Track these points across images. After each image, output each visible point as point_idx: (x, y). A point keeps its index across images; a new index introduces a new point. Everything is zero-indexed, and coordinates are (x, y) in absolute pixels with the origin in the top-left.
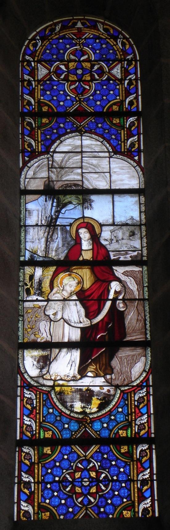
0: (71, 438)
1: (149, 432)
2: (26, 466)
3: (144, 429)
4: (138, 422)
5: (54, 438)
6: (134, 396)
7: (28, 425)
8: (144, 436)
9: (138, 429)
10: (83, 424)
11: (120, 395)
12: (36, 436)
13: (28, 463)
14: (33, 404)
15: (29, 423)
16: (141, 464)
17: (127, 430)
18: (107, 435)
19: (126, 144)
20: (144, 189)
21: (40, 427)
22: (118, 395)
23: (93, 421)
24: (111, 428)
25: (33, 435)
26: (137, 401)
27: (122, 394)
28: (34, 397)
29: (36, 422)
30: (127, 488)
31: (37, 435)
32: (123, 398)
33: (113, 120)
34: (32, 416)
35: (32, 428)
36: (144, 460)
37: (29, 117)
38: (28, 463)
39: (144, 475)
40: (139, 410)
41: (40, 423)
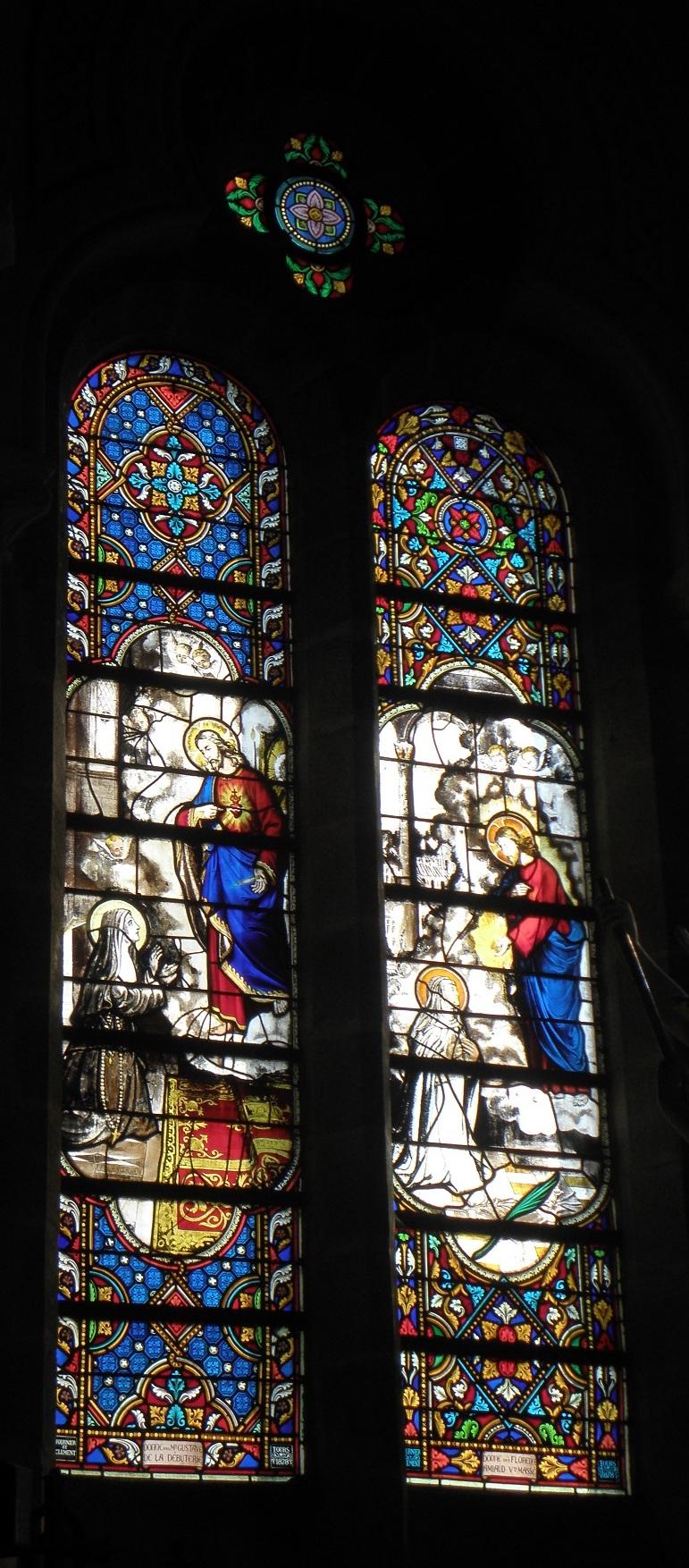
0: (148, 1302)
1: (294, 1302)
2: (64, 1240)
3: (274, 491)
4: (275, 1398)
5: (122, 563)
6: (261, 572)
7: (75, 592)
8: (286, 1309)
9: (276, 1411)
10: (172, 1277)
11: (241, 1219)
12: (81, 1296)
13: (68, 1349)
14: (89, 412)
15: (67, 1269)
16: (280, 1366)
17: (252, 1294)
18: (216, 1303)
19: (266, 1227)
20: (301, 1486)
21: (98, 542)
22: (237, 1220)
23: (191, 1272)
24: (224, 1287)
25: (74, 1294)
26: (266, 580)
27: (244, 1217)
28: (74, 1389)
29: (89, 537)
30: (248, 1395)
31: (84, 1294)
32: (246, 1225)
33: (241, 1332)
34: (81, 524)
35: (71, 1395)
36: (283, 1359)
37: (70, 554)
38: (68, 1349)
39: (270, 521)
40: (268, 549)
41: (97, 536)
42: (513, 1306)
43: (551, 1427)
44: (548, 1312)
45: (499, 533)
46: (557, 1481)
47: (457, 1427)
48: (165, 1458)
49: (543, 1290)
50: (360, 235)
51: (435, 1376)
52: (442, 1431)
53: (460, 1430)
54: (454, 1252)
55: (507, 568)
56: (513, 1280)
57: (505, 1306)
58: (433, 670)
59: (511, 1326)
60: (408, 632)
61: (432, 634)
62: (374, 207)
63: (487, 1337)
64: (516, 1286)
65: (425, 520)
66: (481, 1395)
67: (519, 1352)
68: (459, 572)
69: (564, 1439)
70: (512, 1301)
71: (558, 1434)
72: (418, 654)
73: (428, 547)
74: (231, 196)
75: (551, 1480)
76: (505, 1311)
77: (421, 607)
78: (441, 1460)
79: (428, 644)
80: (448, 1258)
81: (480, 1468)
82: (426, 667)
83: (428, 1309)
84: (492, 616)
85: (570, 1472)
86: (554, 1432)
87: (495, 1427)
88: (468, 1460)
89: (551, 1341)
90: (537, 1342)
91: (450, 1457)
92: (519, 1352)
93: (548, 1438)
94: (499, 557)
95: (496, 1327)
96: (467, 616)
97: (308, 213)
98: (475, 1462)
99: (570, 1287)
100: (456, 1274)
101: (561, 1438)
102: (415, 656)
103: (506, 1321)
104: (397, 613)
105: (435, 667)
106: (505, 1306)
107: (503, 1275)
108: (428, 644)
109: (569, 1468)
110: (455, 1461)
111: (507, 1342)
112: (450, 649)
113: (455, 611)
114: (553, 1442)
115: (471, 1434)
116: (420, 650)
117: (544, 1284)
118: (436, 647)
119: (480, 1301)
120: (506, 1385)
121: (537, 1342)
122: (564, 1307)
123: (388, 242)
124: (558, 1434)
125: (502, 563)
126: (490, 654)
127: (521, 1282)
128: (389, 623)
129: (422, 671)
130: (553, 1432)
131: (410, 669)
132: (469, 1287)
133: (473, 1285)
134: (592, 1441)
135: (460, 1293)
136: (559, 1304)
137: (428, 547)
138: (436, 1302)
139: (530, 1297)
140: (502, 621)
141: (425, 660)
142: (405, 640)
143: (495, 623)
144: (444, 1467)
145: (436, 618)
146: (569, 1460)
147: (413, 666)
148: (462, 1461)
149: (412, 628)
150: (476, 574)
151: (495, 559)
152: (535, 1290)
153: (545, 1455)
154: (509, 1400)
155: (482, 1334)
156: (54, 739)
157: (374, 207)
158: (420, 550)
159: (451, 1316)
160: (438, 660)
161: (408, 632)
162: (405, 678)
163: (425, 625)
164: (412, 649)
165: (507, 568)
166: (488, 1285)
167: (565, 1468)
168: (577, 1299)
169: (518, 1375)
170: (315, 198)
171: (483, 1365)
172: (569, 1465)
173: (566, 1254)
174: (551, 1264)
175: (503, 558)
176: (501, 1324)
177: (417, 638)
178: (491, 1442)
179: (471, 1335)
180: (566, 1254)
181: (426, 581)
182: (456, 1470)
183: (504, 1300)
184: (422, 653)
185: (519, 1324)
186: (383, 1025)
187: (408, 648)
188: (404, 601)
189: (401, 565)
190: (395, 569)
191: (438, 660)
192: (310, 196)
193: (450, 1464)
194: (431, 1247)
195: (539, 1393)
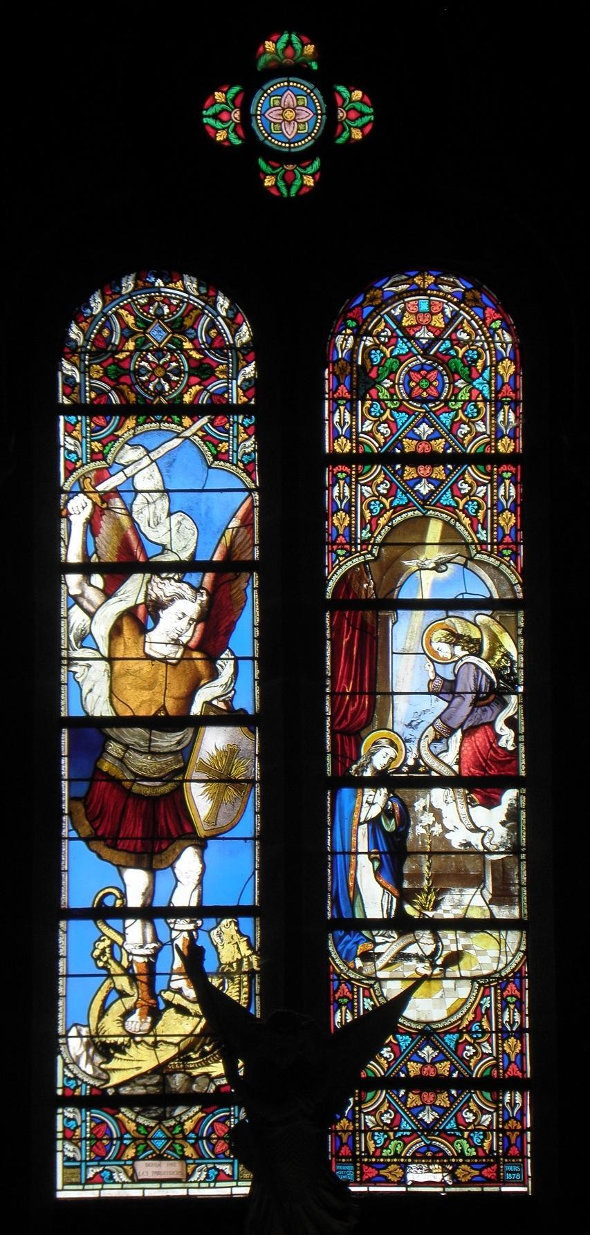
42: (435, 1048)
43: (465, 1142)
44: (465, 1050)
45: (455, 387)
46: (470, 1183)
47: (385, 1147)
50: (332, 125)
51: (365, 1108)
52: (372, 1149)
53: (387, 1148)
54: (467, 530)
55: (461, 419)
56: (434, 1027)
57: (428, 1049)
58: (463, 1017)
59: (433, 1063)
61: (388, 490)
62: (346, 93)
65: (386, 386)
66: (405, 1120)
68: (416, 430)
70: (435, 1044)
71: (471, 1147)
73: (388, 411)
74: (284, 191)
75: (465, 1182)
76: (428, 1052)
77: (380, 467)
78: (371, 1172)
79: (469, 1039)
81: (404, 1177)
82: (470, 1017)
83: (489, 486)
84: (445, 466)
85: (481, 1175)
86: (468, 1146)
87: (417, 1144)
88: (393, 1172)
90: (398, 466)
91: (378, 1170)
93: (462, 1150)
94: (453, 410)
95: (433, 323)
97: (289, 122)
98: (400, 1173)
101: (473, 1149)
103: (424, 328)
104: (358, 475)
105: (461, 1019)
106: (428, 1049)
107: (428, 1023)
108: (469, 1039)
109: (481, 1173)
110: (382, 1172)
111: (428, 1092)
113: (411, 466)
114: (467, 1154)
115: (396, 1151)
116: (476, 1032)
118: (461, 1037)
121: (455, 1075)
123: (356, 127)
125: (456, 416)
128: (350, 486)
129: (378, 525)
130: (466, 1146)
131: (366, 524)
133: (450, 506)
134: (501, 1151)
137: (388, 411)
138: (481, 490)
139: (451, 1039)
140: (454, 469)
143: (448, 472)
144: (373, 1177)
145: (393, 475)
146: (480, 1166)
147: (370, 522)
148: (390, 1172)
151: (449, 412)
152: (453, 1033)
154: (428, 1047)
155: (407, 1073)
156: (128, 582)
157: (346, 93)
158: (382, 415)
159: (470, 481)
162: (361, 533)
164: (484, 1032)
165: (461, 419)
167: (477, 1173)
168: (491, 1036)
170: (289, 98)
171: (407, 1097)
172: (481, 1170)
173: (482, 1002)
174: (468, 1012)
175: (457, 410)
176: (424, 1063)
177: (374, 496)
178: (413, 1157)
179: (398, 1073)
180: (482, 1002)
181: (468, 1101)
182: (383, 1179)
183: (428, 1044)
184: (474, 1030)
185: (440, 1062)
190: (497, 1110)
191: (393, 513)
192: (295, 130)
193: (378, 1175)
195: (455, 1115)
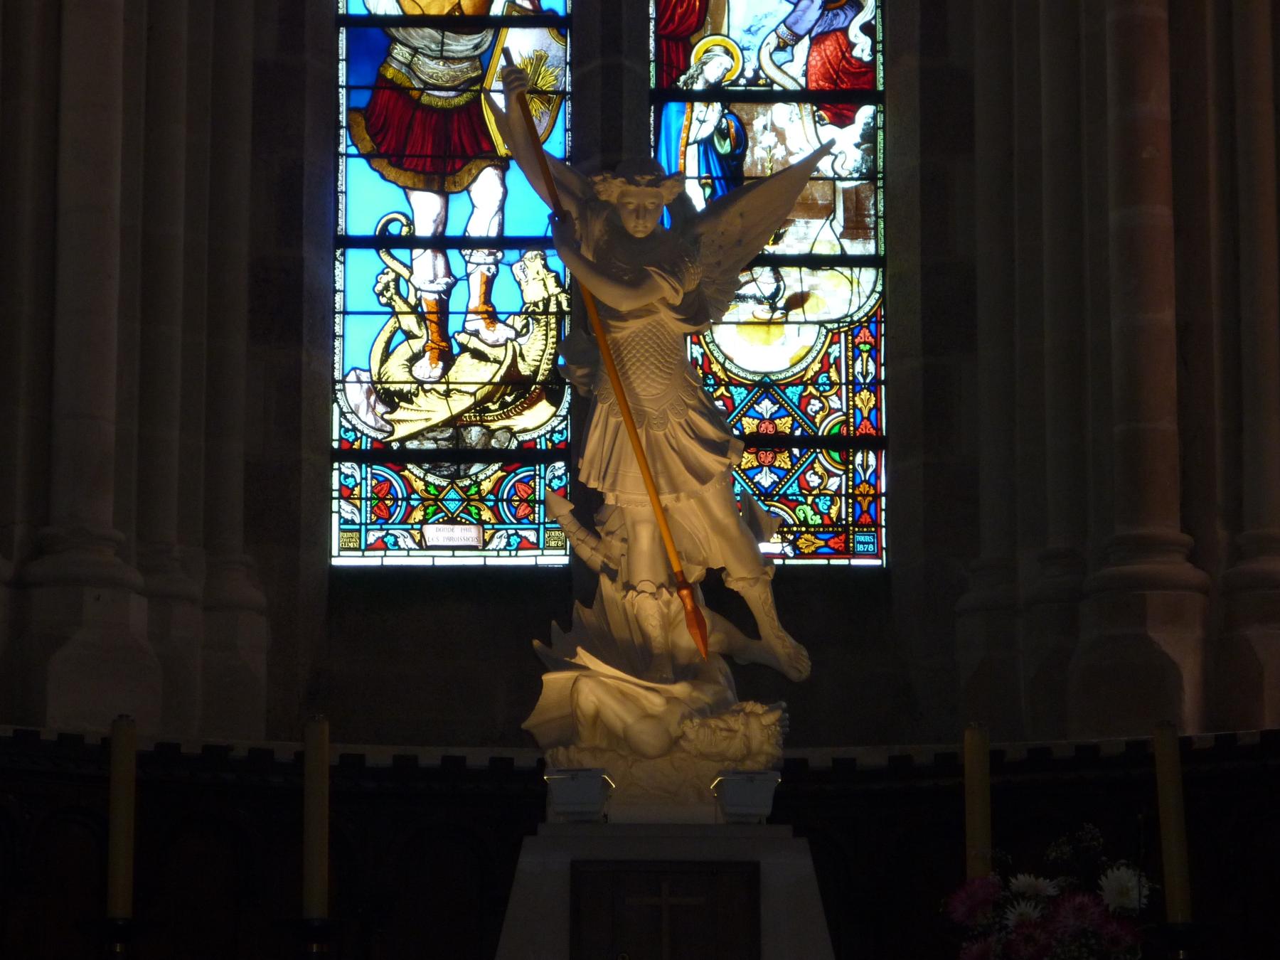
48: (435, 539)
49: (806, 385)
56: (774, 378)
59: (772, 419)
60: (835, 403)
63: (747, 431)
64: (774, 383)
67: (778, 442)
69: (822, 518)
71: (815, 514)
72: (825, 379)
75: (809, 554)
77: (820, 434)
80: (710, 363)
82: (816, 366)
86: (812, 512)
89: (813, 431)
92: (778, 442)
93: (805, 518)
96: (771, 430)
99: (833, 379)
100: (719, 377)
101: (818, 517)
102: (829, 378)
105: (806, 369)
108: (814, 392)
112: (789, 391)
116: (824, 384)
117: (805, 379)
118: (805, 390)
119: (742, 401)
120: (769, 413)
122: (826, 398)
124: (815, 514)
126: (746, 392)
127: (781, 380)
130: (810, 513)
132: (732, 388)
135: (722, 394)
136: (821, 395)
141: (817, 374)
142: (838, 394)
147: (830, 366)
149: (830, 408)
150: (757, 479)
152: (797, 385)
153: (802, 533)
154: (767, 400)
160: (803, 376)
161: (835, 403)
163: (817, 412)
164: (832, 384)
166: (749, 387)
168: (840, 389)
169: (777, 464)
180: (830, 350)
181: (813, 462)
186: (552, 206)
187: (837, 384)
188: (839, 434)
189: (840, 476)
190: (846, 472)
191: (803, 376)
194: (694, 356)
